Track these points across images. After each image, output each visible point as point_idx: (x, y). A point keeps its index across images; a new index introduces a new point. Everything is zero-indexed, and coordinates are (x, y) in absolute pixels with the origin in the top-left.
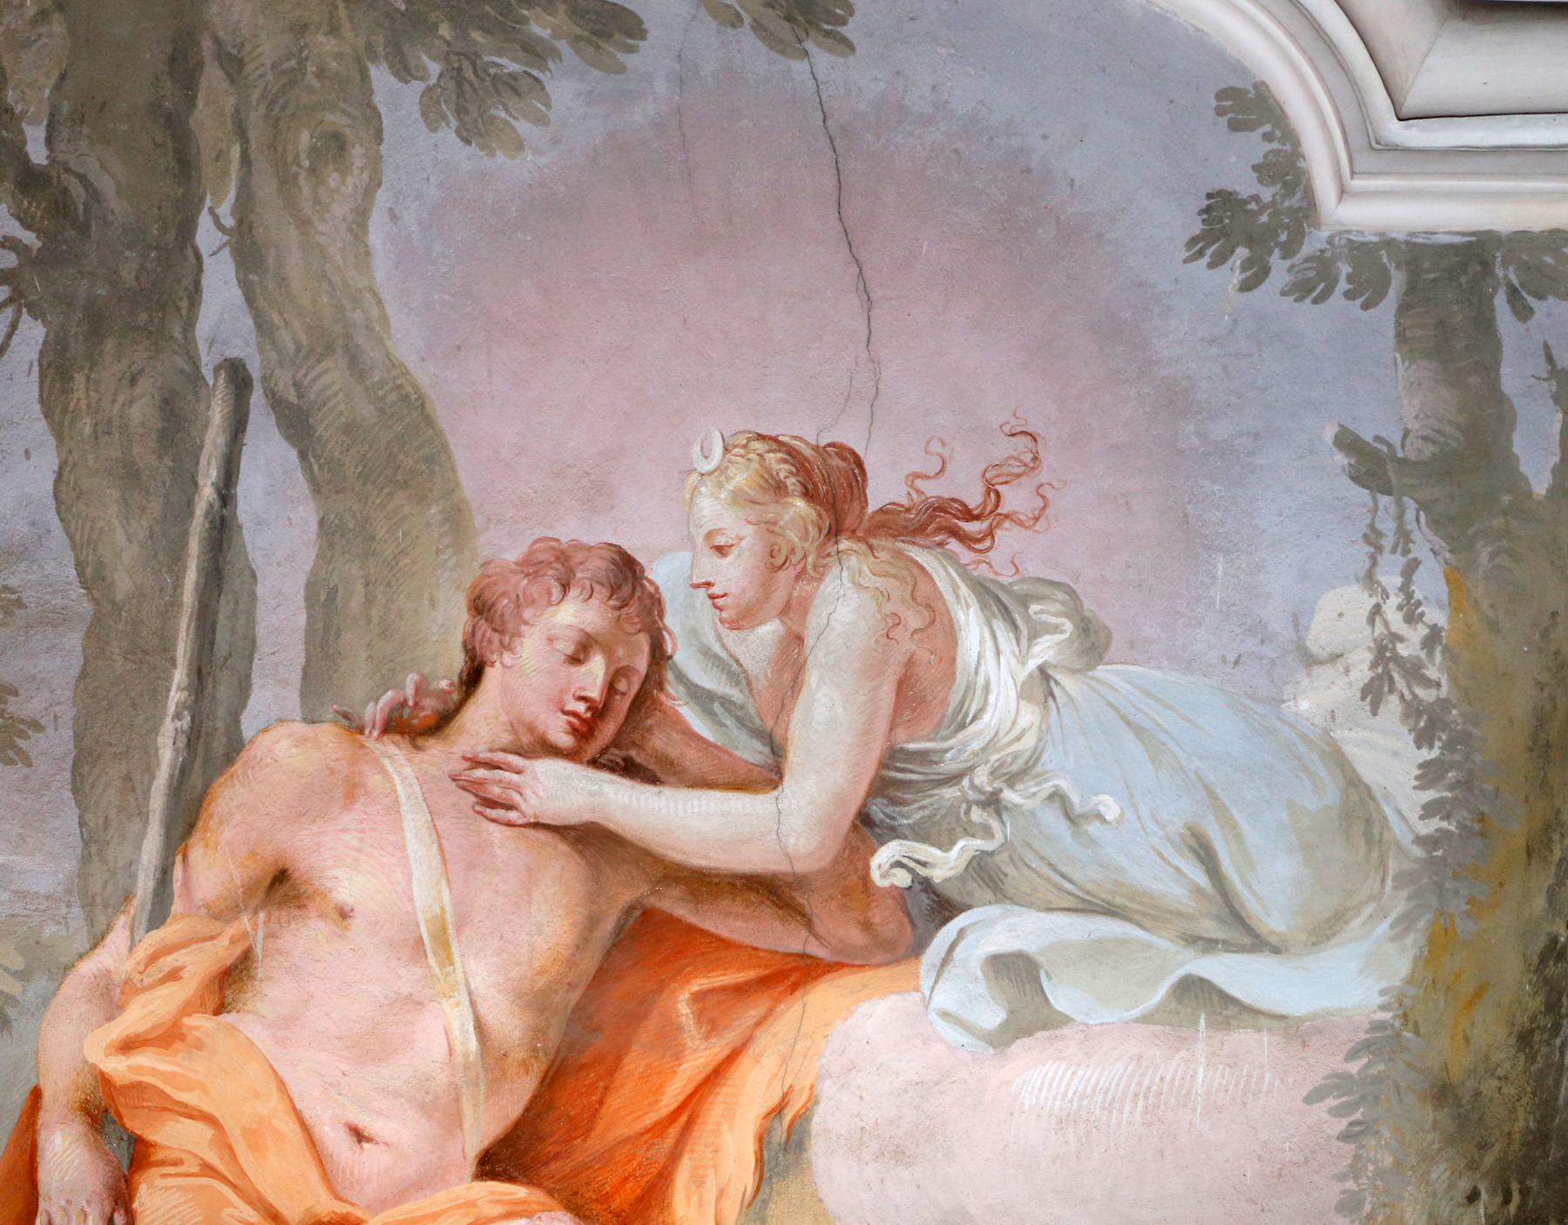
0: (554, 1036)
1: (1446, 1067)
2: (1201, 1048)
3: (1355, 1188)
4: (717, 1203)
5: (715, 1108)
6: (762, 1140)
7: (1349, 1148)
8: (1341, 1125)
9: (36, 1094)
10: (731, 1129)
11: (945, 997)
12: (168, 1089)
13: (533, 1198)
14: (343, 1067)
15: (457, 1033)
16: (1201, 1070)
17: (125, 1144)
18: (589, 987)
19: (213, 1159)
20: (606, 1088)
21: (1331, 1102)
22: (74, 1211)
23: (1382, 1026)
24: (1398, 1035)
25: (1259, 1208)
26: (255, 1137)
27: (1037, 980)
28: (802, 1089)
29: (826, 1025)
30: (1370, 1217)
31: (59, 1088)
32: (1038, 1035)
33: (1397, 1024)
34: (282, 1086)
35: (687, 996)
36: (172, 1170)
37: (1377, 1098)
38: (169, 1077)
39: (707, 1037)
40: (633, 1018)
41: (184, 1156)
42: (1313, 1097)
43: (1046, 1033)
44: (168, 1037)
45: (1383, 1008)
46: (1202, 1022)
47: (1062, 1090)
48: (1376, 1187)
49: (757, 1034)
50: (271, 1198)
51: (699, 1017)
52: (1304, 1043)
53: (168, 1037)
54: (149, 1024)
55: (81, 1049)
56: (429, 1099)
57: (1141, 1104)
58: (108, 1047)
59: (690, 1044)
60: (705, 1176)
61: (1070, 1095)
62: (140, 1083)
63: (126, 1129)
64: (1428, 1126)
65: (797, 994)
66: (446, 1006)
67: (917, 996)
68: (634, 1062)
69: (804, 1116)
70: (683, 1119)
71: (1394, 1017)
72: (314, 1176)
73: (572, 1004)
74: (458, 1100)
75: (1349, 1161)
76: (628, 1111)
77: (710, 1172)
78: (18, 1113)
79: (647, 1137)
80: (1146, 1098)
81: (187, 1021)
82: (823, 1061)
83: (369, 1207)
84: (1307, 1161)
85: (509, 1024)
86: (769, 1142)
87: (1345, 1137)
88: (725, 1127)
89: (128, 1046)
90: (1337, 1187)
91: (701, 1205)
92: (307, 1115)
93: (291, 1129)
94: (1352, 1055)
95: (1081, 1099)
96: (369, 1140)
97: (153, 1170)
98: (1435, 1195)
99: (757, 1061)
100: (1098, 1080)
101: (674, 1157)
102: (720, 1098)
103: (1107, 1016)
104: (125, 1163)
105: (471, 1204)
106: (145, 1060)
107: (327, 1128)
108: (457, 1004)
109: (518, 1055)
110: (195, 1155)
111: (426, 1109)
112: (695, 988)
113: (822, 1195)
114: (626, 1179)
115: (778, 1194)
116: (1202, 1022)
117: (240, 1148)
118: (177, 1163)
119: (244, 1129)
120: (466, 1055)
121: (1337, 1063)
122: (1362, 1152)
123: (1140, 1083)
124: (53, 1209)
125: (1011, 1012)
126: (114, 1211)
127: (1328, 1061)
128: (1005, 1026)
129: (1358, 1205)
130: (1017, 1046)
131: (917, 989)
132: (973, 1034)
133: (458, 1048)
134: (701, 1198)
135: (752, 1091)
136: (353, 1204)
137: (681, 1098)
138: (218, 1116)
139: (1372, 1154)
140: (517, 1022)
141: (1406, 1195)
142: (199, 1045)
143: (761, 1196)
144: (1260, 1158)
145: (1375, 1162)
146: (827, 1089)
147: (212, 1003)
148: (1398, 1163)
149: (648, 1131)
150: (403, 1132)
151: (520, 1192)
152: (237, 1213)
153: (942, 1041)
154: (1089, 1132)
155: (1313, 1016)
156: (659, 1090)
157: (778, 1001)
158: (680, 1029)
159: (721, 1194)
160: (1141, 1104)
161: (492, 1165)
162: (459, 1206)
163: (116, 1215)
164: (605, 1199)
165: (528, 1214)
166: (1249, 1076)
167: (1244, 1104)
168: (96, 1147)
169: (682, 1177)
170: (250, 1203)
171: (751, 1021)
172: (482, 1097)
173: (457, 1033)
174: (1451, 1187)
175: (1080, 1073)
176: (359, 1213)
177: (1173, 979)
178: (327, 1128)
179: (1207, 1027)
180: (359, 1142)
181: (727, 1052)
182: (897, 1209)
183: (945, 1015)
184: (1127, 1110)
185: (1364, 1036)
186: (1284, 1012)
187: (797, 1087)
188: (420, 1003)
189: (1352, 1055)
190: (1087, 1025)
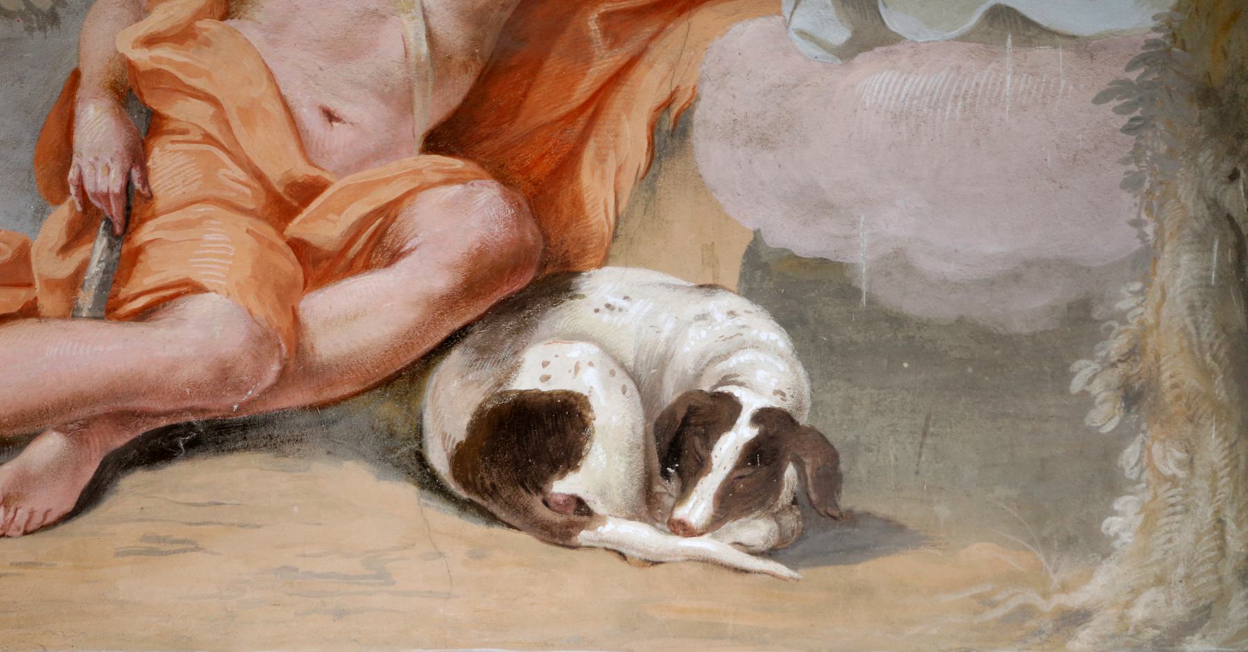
0: (489, 43)
1: (1208, 75)
2: (1009, 61)
3: (1136, 170)
4: (617, 174)
5: (617, 101)
6: (654, 128)
7: (1131, 139)
8: (1124, 120)
9: (76, 75)
10: (628, 119)
11: (801, 20)
12: (181, 76)
13: (468, 169)
14: (321, 63)
15: (412, 40)
16: (1009, 78)
17: (143, 116)
18: (518, 8)
19: (213, 130)
20: (530, 85)
21: (1115, 103)
22: (100, 165)
23: (1156, 43)
24: (1168, 51)
25: (1058, 185)
26: (247, 115)
27: (876, 8)
28: (687, 88)
29: (707, 40)
30: (1149, 192)
31: (95, 69)
32: (877, 50)
33: (1168, 42)
34: (271, 76)
35: (596, 16)
36: (180, 138)
37: (1152, 99)
38: (182, 66)
39: (611, 47)
40: (553, 32)
41: (190, 127)
42: (1102, 98)
43: (884, 49)
44: (183, 35)
45: (1156, 29)
46: (1009, 41)
47: (896, 92)
48: (1154, 169)
49: (651, 46)
50: (258, 162)
51: (605, 32)
52: (1092, 57)
53: (183, 35)
54: (169, 25)
55: (114, 42)
56: (387, 90)
57: (960, 103)
58: (136, 41)
59: (597, 52)
60: (607, 155)
61: (903, 96)
62: (159, 70)
63: (145, 105)
64: (1195, 121)
65: (685, 15)
66: (405, 19)
67: (779, 18)
68: (553, 65)
69: (688, 110)
70: (590, 110)
71: (1165, 37)
72: (293, 147)
73: (504, 20)
74: (410, 91)
75: (1131, 149)
76: (546, 103)
77: (612, 153)
78: (61, 89)
79: (561, 123)
80: (965, 99)
81: (199, 24)
82: (704, 67)
83: (335, 172)
84: (1096, 148)
85: (453, 34)
86: (659, 130)
87: (1127, 130)
88: (624, 117)
89: (151, 41)
90: (1123, 169)
91: (603, 177)
92: (290, 99)
93: (276, 109)
94: (1128, 69)
95: (912, 99)
96: (338, 120)
97: (165, 138)
98: (1202, 175)
99: (651, 67)
100: (925, 86)
101: (583, 139)
102: (620, 95)
103: (932, 35)
104: (143, 131)
105: (417, 172)
106: (165, 53)
107: (305, 110)
108: (413, 18)
109: (460, 58)
110: (199, 127)
111: (385, 98)
112: (603, 10)
113: (701, 172)
114: (543, 156)
115: (666, 170)
116: (1009, 41)
117: (235, 124)
118: (184, 132)
119: (239, 109)
120: (418, 57)
121: (1119, 72)
122: (1142, 142)
123: (959, 88)
124: (84, 164)
125: (855, 32)
126: (131, 167)
127: (1113, 71)
128: (850, 42)
129: (1141, 182)
130: (859, 59)
131: (779, 13)
132: (825, 49)
133: (412, 52)
134: (603, 172)
135: (649, 87)
136: (323, 170)
137: (589, 94)
138: (219, 98)
139: (1149, 143)
140: (460, 33)
141: (1178, 175)
142: (207, 43)
143: (652, 171)
144: (1058, 146)
145: (1153, 149)
146: (707, 90)
147: (219, 11)
148: (1171, 150)
149: (562, 118)
150: (365, 115)
151: (457, 164)
152: (229, 173)
153: (800, 54)
154: (918, 126)
155: (1099, 36)
156: (571, 88)
157: (668, 21)
158: (589, 41)
159: (619, 170)
160: (960, 103)
161: (435, 142)
162: (408, 174)
163: (133, 171)
164: (526, 171)
165: (463, 181)
166: (1048, 82)
167: (1045, 104)
168: (120, 117)
169: (588, 155)
170: (241, 166)
171: (647, 36)
172: (430, 90)
173: (412, 40)
174: (1215, 169)
175: (911, 79)
176: (327, 176)
177: (984, 8)
178: (305, 110)
179: (1014, 44)
180: (330, 121)
181: (627, 59)
182: (762, 183)
183: (802, 33)
184: (949, 108)
185: (1141, 52)
186: (1076, 34)
187: (682, 88)
188: (384, 17)
189: (1131, 67)
190: (916, 43)
